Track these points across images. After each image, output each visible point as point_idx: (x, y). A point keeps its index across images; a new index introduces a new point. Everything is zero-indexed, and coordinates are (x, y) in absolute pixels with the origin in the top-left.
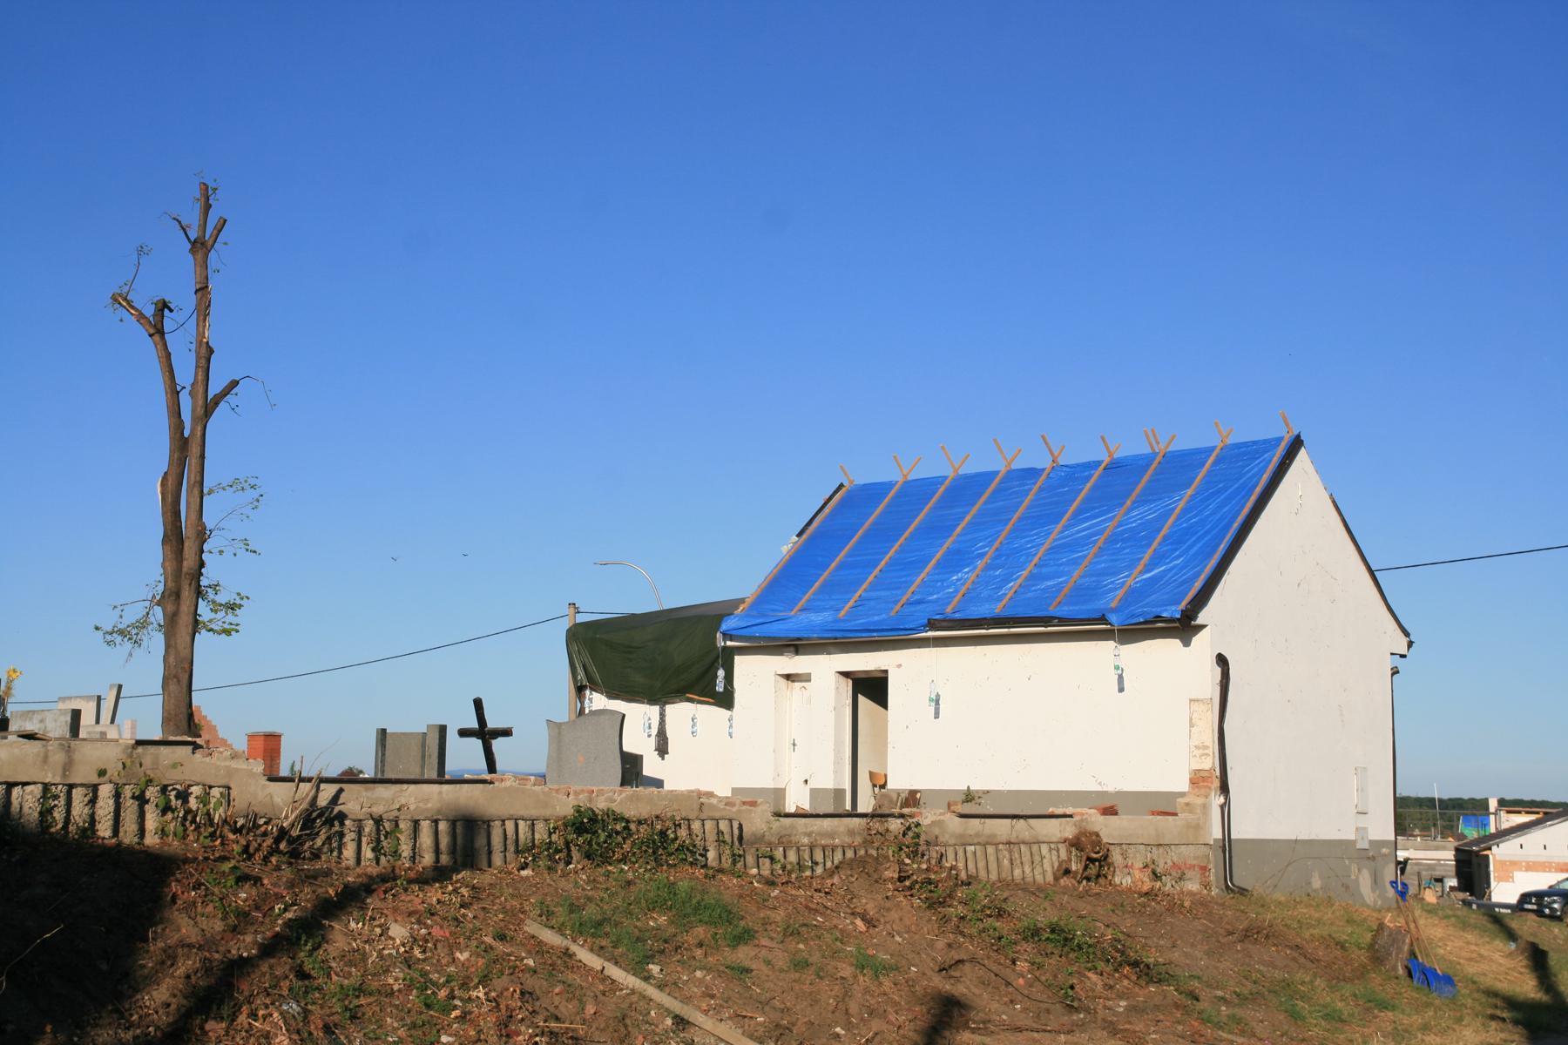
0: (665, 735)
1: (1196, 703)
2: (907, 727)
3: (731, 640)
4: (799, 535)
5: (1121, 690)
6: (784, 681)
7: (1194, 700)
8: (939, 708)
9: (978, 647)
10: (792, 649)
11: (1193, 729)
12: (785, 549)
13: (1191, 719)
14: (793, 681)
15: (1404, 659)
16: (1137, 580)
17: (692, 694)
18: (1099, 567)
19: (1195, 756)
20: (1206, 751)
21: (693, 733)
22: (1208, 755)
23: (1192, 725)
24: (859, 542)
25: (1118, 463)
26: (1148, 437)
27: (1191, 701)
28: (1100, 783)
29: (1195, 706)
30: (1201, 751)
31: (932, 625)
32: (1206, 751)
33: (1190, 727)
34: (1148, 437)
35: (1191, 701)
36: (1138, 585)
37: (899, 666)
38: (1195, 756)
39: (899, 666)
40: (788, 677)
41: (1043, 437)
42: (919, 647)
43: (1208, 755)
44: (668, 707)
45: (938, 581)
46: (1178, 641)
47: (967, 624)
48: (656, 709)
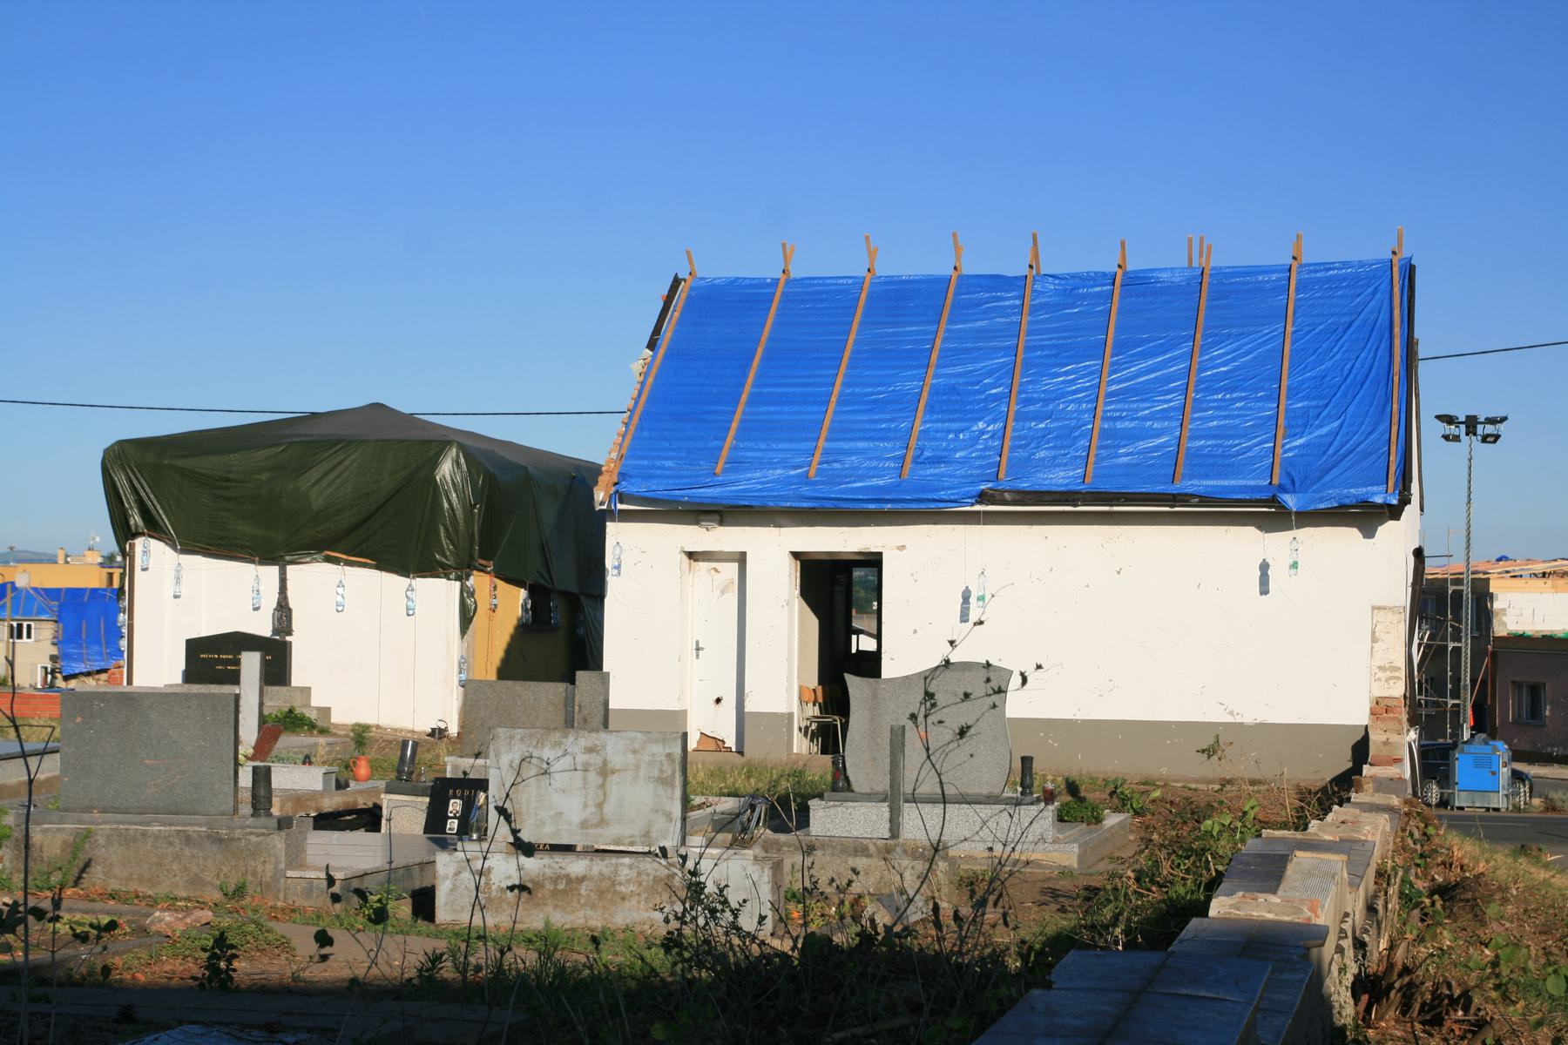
0: (287, 603)
1: (1382, 612)
2: (915, 632)
3: (622, 502)
4: (652, 345)
5: (1264, 590)
6: (685, 559)
7: (1379, 608)
8: (968, 609)
9: (1034, 527)
10: (717, 517)
11: (1376, 645)
12: (637, 367)
13: (1373, 633)
14: (696, 560)
15: (1498, 557)
16: (1288, 446)
17: (333, 551)
18: (1211, 424)
19: (1379, 679)
20: (1397, 674)
21: (408, 609)
22: (1399, 678)
23: (1374, 640)
24: (762, 366)
25: (1138, 278)
26: (1190, 247)
27: (1374, 608)
28: (1231, 713)
29: (1380, 616)
30: (1388, 674)
31: (983, 498)
32: (1397, 674)
33: (1373, 642)
34: (1190, 247)
35: (1374, 608)
36: (1290, 454)
37: (902, 548)
38: (1379, 679)
39: (902, 548)
40: (692, 556)
41: (688, 252)
42: (935, 523)
43: (1399, 678)
44: (291, 570)
45: (949, 432)
46: (1253, 528)
47: (1047, 498)
48: (274, 571)
